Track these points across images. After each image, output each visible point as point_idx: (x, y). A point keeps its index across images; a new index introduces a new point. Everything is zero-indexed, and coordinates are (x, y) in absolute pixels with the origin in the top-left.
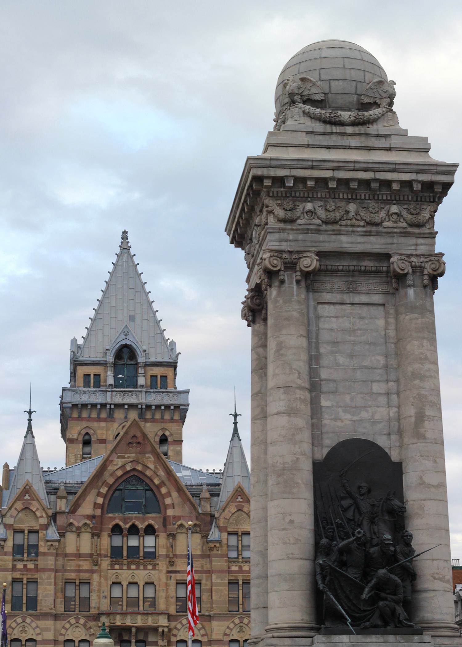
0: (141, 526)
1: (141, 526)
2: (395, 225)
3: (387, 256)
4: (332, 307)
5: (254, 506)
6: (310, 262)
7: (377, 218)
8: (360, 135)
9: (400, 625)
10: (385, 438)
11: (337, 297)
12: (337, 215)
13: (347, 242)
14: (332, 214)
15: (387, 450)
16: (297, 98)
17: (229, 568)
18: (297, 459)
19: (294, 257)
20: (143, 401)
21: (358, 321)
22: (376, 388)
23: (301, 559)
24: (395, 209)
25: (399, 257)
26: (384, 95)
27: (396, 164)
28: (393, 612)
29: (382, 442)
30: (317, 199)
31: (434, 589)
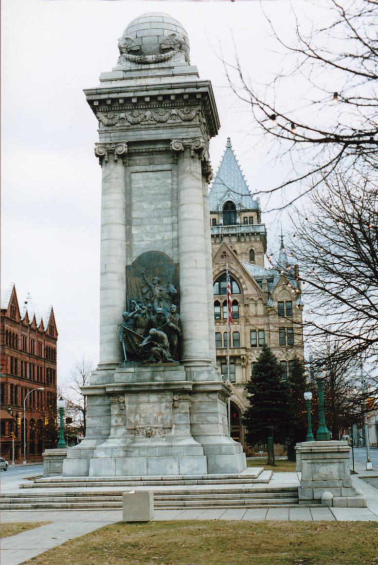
0: (222, 302)
1: (222, 302)
2: (174, 121)
3: (168, 141)
4: (140, 174)
6: (123, 149)
7: (164, 119)
8: (159, 68)
11: (143, 168)
12: (139, 119)
13: (145, 135)
14: (136, 119)
16: (124, 50)
17: (279, 321)
19: (112, 146)
20: (239, 232)
21: (155, 181)
22: (165, 220)
24: (174, 111)
25: (175, 141)
26: (176, 42)
27: (171, 84)
28: (161, 352)
29: (168, 252)
30: (128, 110)
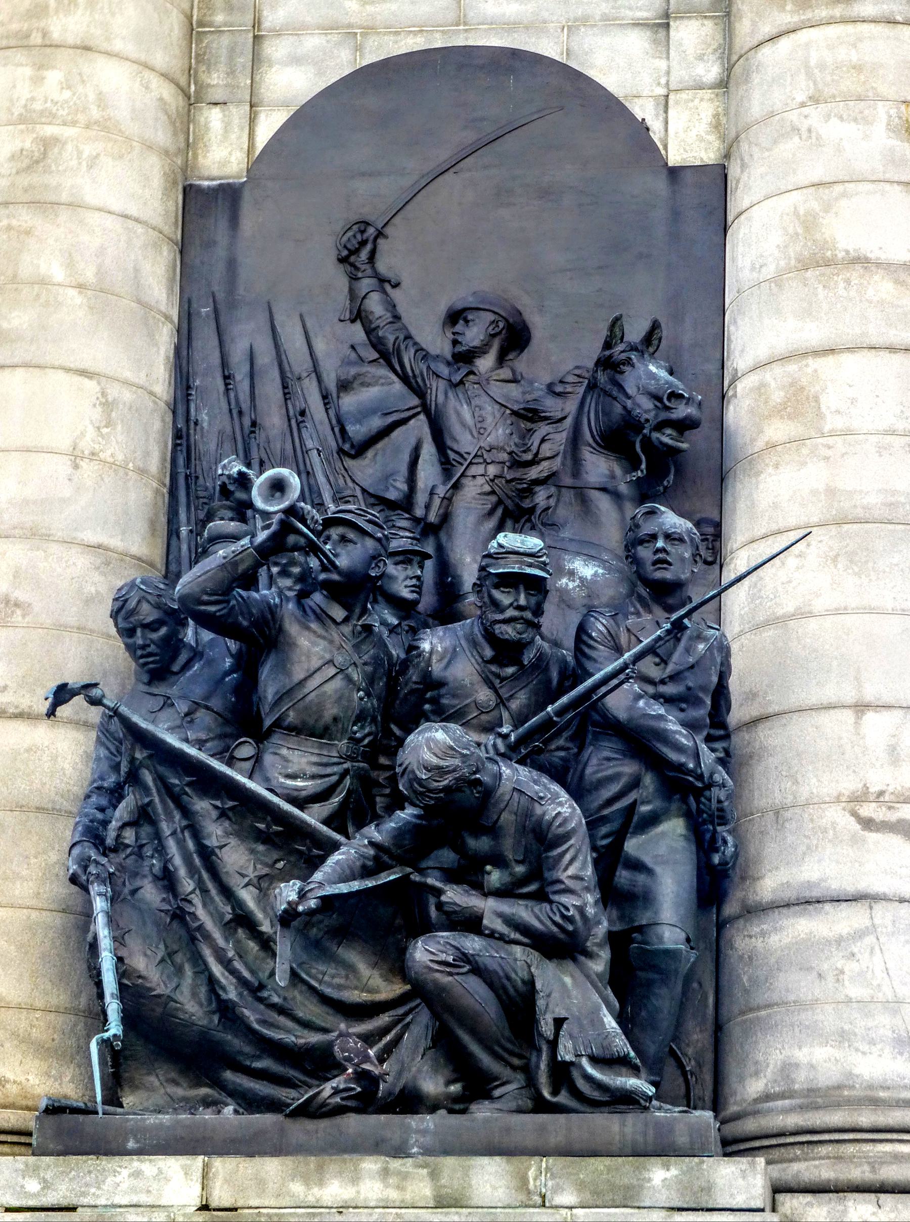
9: (563, 1098)
10: (637, 42)
15: (643, 110)
18: (47, 144)
28: (520, 1005)
31: (864, 884)
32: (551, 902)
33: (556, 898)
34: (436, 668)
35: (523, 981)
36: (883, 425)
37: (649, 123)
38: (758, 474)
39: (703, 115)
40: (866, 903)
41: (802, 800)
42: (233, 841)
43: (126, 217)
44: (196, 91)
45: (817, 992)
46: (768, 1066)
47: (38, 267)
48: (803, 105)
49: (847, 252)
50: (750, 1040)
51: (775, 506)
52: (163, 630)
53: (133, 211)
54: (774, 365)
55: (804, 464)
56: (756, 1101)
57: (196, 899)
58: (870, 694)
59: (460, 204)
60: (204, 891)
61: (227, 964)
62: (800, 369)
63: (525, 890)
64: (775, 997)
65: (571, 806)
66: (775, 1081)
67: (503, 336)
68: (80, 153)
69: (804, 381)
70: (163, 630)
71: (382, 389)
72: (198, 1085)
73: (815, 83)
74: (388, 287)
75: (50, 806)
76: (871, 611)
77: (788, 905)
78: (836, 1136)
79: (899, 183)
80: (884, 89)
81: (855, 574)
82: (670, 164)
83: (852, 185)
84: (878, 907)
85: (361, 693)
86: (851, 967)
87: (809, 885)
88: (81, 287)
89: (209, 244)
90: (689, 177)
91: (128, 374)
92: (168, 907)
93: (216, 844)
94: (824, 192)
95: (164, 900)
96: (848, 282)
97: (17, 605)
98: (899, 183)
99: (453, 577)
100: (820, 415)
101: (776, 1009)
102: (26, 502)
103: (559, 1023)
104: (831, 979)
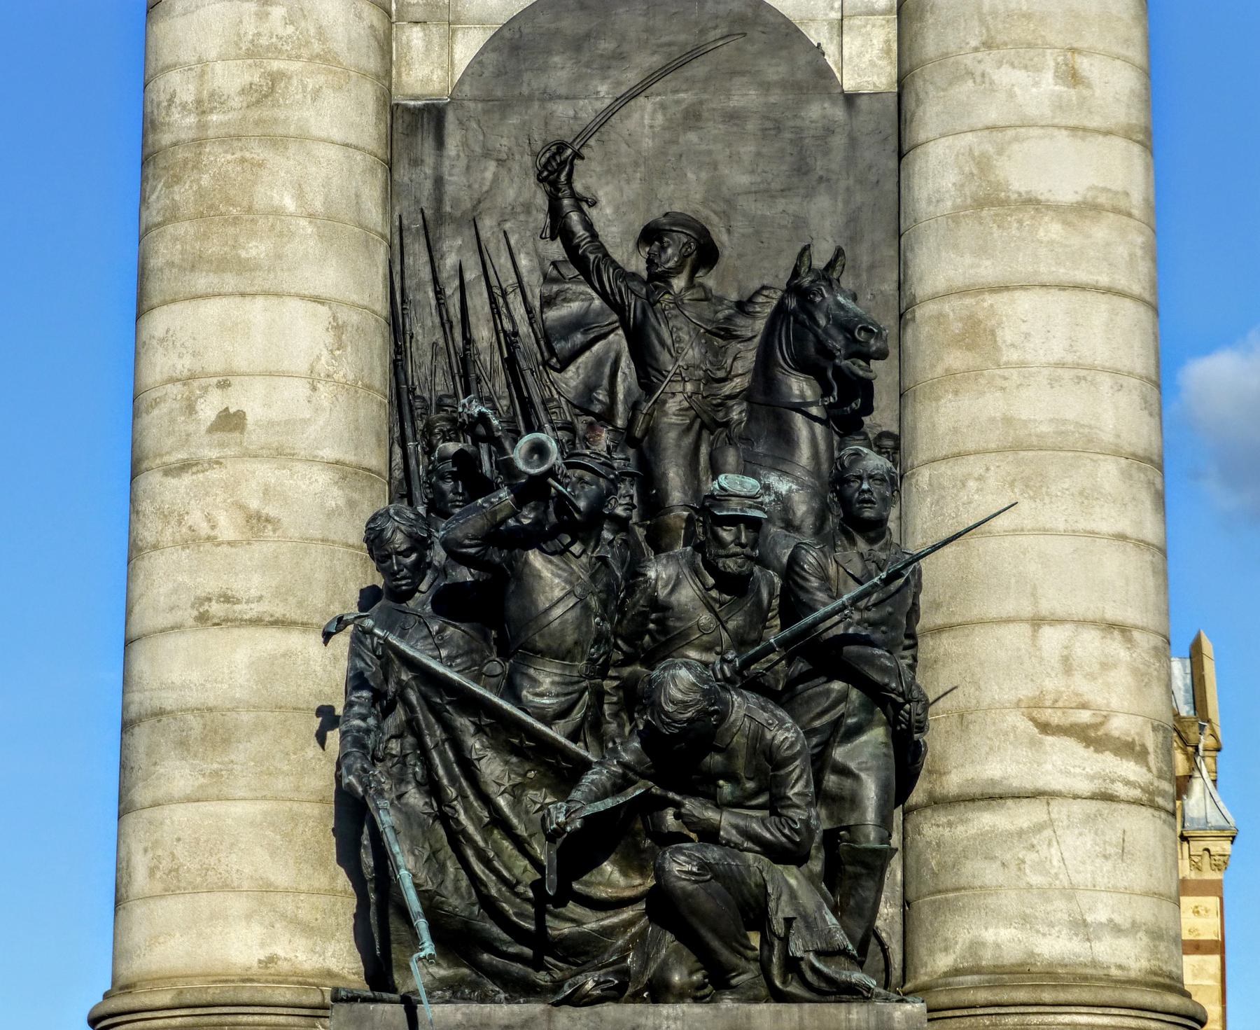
5: (847, 254)
9: (794, 988)
15: (817, 34)
18: (275, 79)
23: (982, 622)
28: (754, 911)
31: (1041, 783)
32: (780, 815)
33: (785, 812)
34: (662, 593)
35: (757, 885)
36: (1053, 359)
37: (824, 47)
38: (938, 399)
39: (875, 41)
40: (1044, 799)
41: (984, 705)
42: (490, 754)
43: (347, 145)
44: (397, 10)
45: (1001, 879)
46: (956, 943)
47: (272, 198)
48: (976, 50)
49: (1020, 194)
50: (940, 919)
51: (955, 430)
52: (414, 556)
53: (352, 140)
54: (952, 297)
55: (982, 393)
56: (946, 974)
57: (458, 806)
58: (1045, 608)
59: (651, 127)
60: (465, 797)
61: (487, 863)
62: (977, 303)
63: (754, 803)
64: (963, 882)
65: (796, 731)
66: (964, 957)
67: (693, 256)
68: (304, 87)
69: (981, 316)
70: (414, 556)
71: (582, 300)
72: (459, 965)
73: (988, 30)
74: (585, 207)
75: (304, 706)
76: (1045, 531)
77: (973, 800)
78: (1022, 1009)
79: (1066, 128)
80: (1051, 38)
81: (1031, 498)
82: (845, 88)
83: (1023, 130)
84: (1056, 804)
85: (598, 619)
86: (1031, 857)
87: (993, 782)
88: (311, 216)
89: (416, 162)
90: (863, 103)
91: (354, 297)
92: (430, 811)
93: (474, 757)
94: (998, 136)
95: (426, 803)
96: (1020, 222)
97: (268, 520)
98: (1066, 128)
99: (658, 490)
100: (997, 349)
101: (963, 892)
102: (271, 424)
103: (788, 922)
104: (1013, 867)
